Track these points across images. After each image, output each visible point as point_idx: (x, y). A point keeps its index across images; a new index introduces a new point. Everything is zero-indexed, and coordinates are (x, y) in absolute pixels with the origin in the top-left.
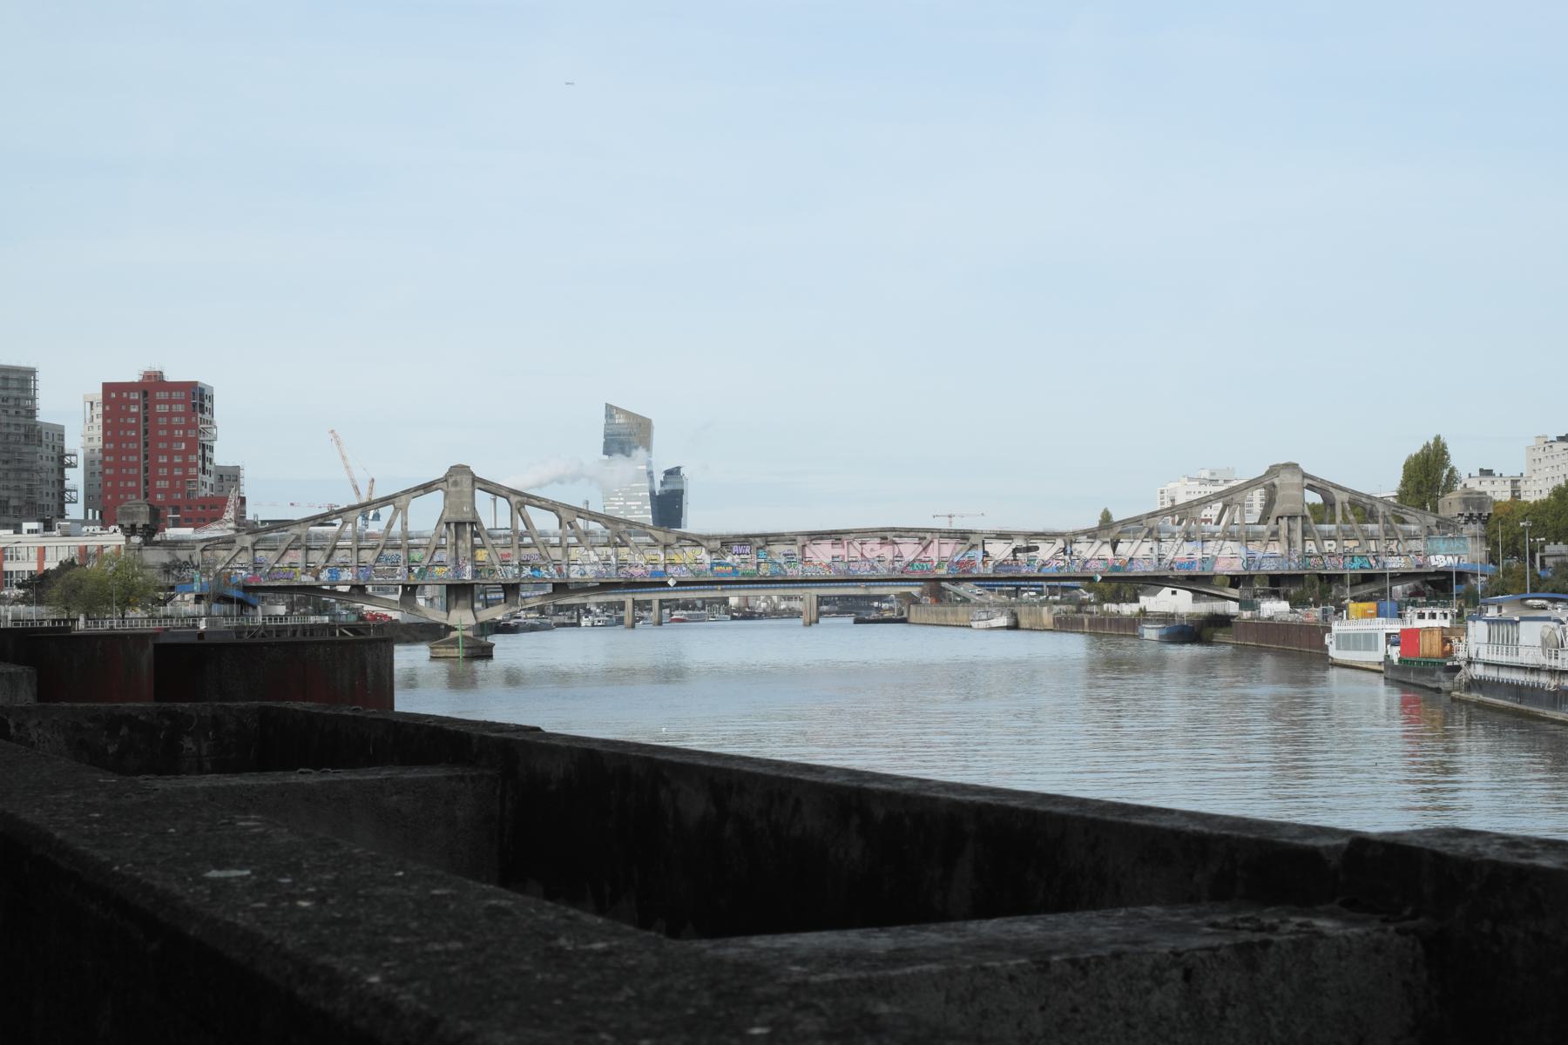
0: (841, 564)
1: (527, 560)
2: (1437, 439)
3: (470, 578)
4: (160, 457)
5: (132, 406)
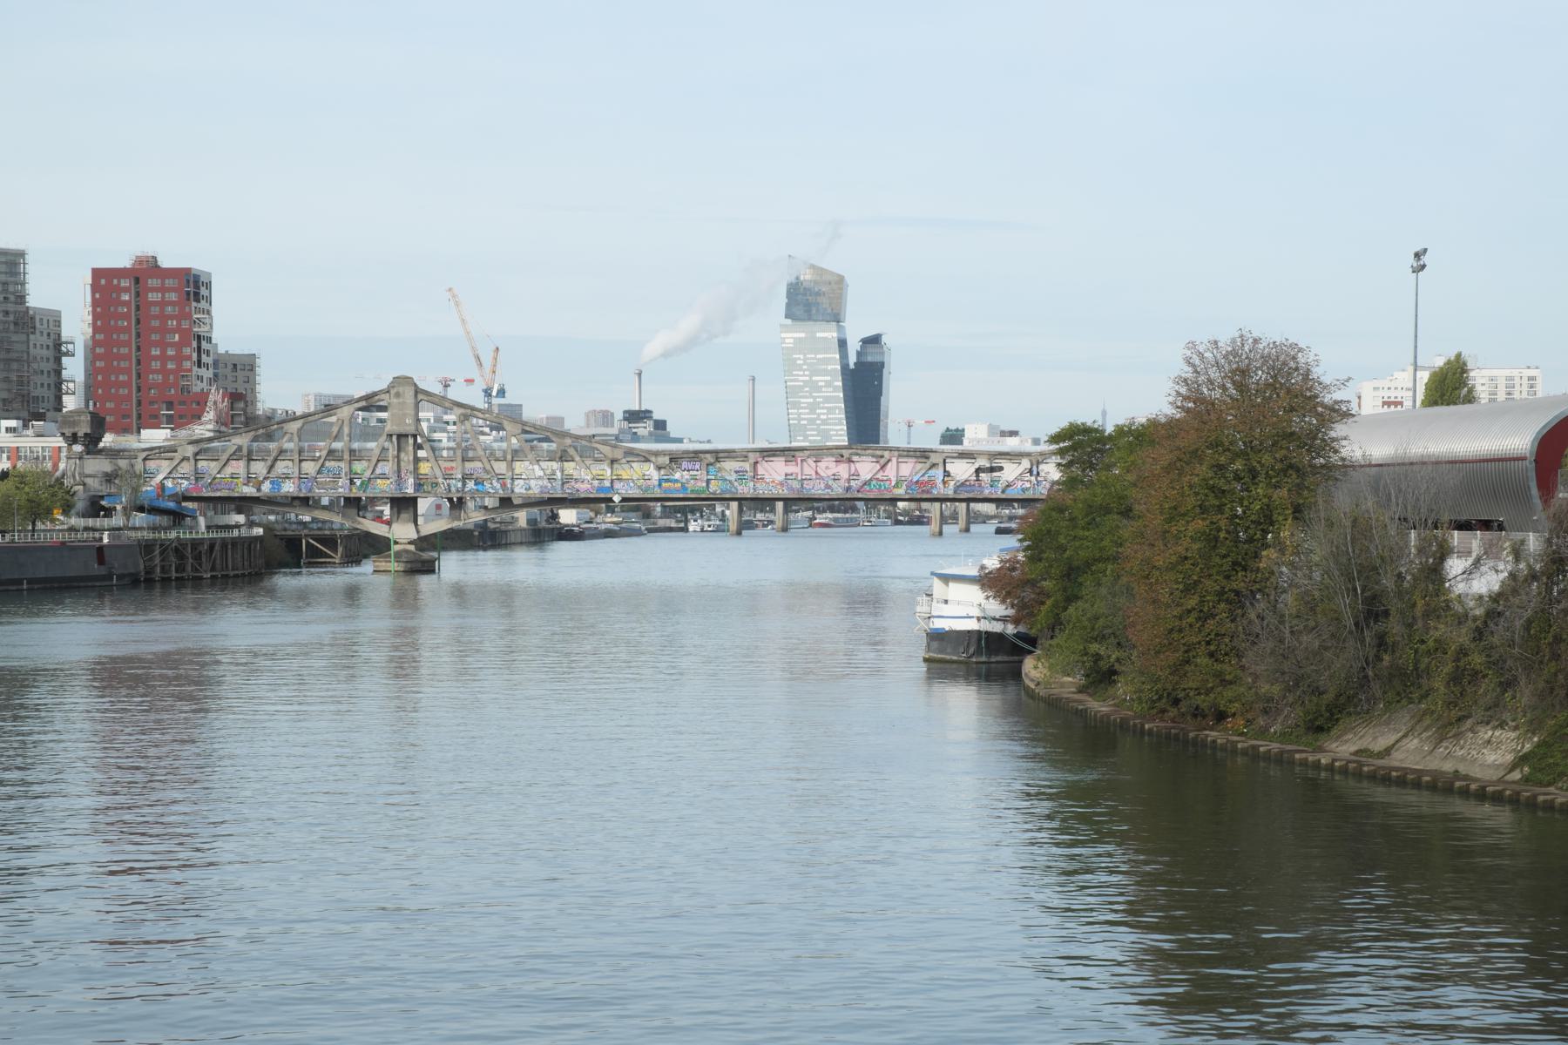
0: (796, 482)
1: (471, 474)
2: (1459, 356)
3: (412, 491)
4: (153, 349)
5: (123, 294)
